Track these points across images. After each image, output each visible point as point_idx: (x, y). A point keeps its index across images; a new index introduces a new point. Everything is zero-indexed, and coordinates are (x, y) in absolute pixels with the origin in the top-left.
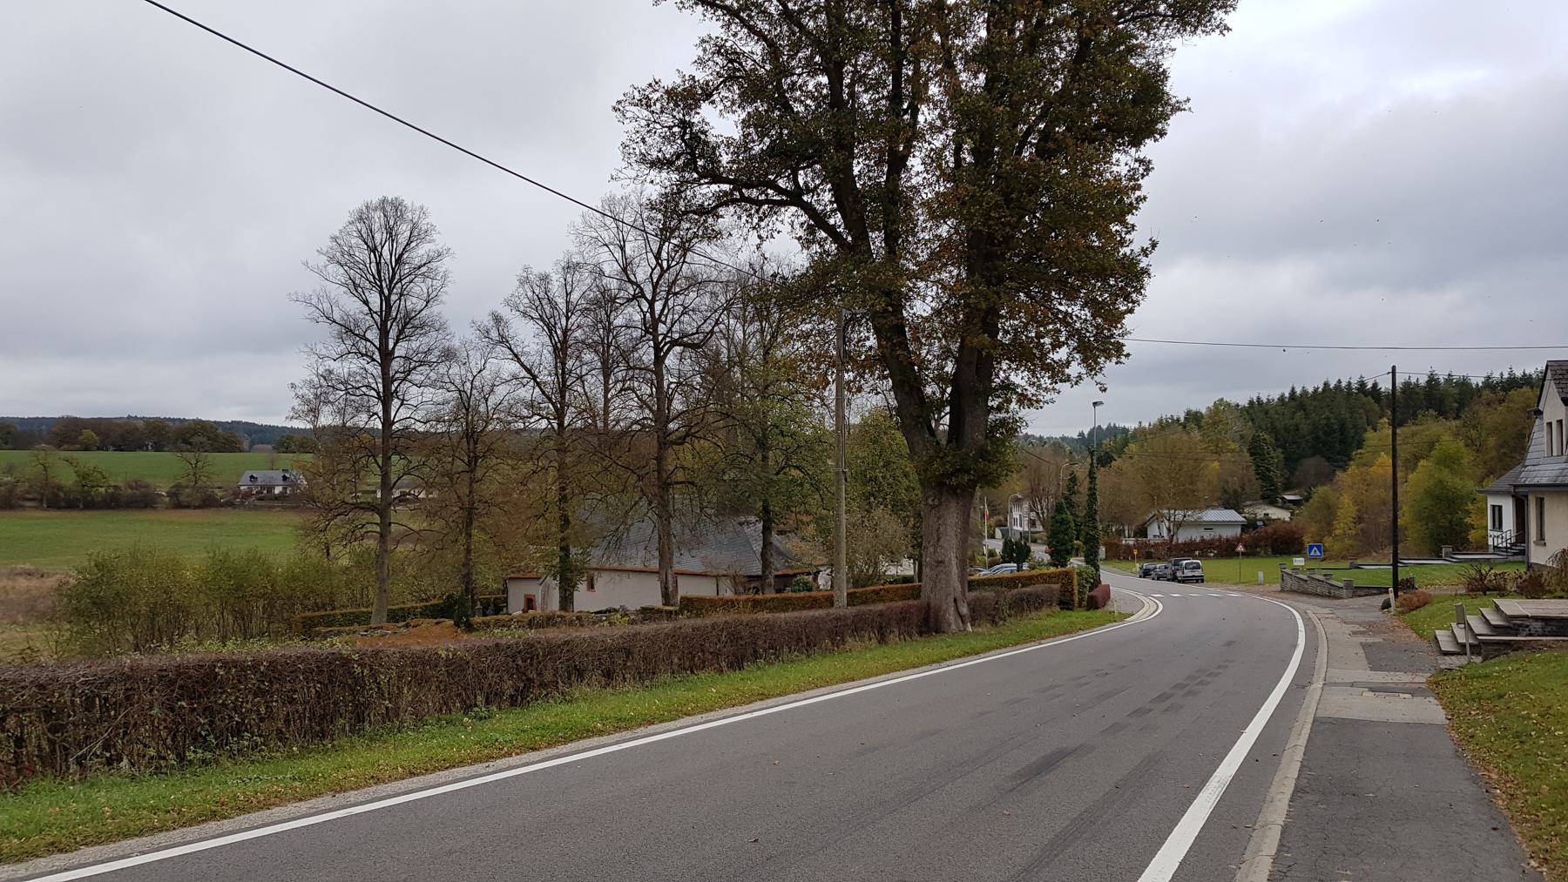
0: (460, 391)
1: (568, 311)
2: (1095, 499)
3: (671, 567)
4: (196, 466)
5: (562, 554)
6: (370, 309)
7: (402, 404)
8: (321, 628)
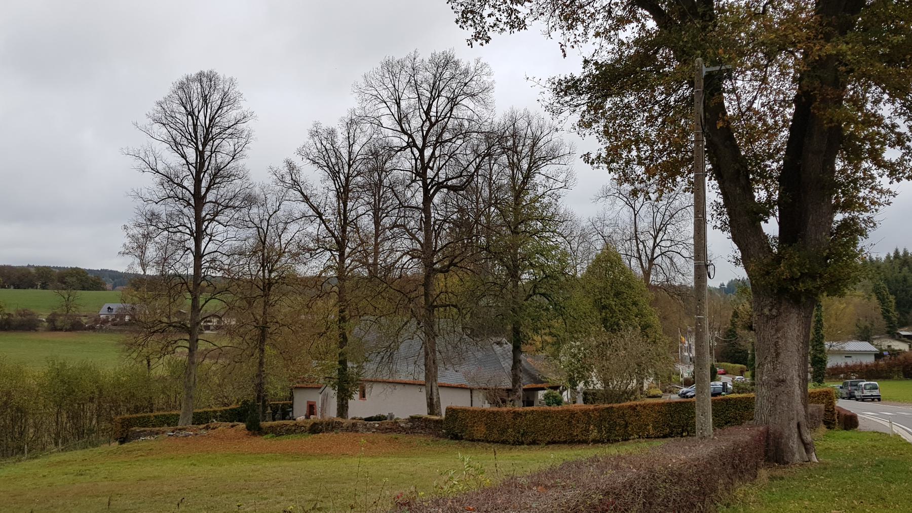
0: (258, 228)
1: (350, 159)
2: (822, 325)
3: (436, 380)
4: (68, 300)
5: (340, 367)
6: (187, 162)
7: (210, 241)
8: (136, 428)
